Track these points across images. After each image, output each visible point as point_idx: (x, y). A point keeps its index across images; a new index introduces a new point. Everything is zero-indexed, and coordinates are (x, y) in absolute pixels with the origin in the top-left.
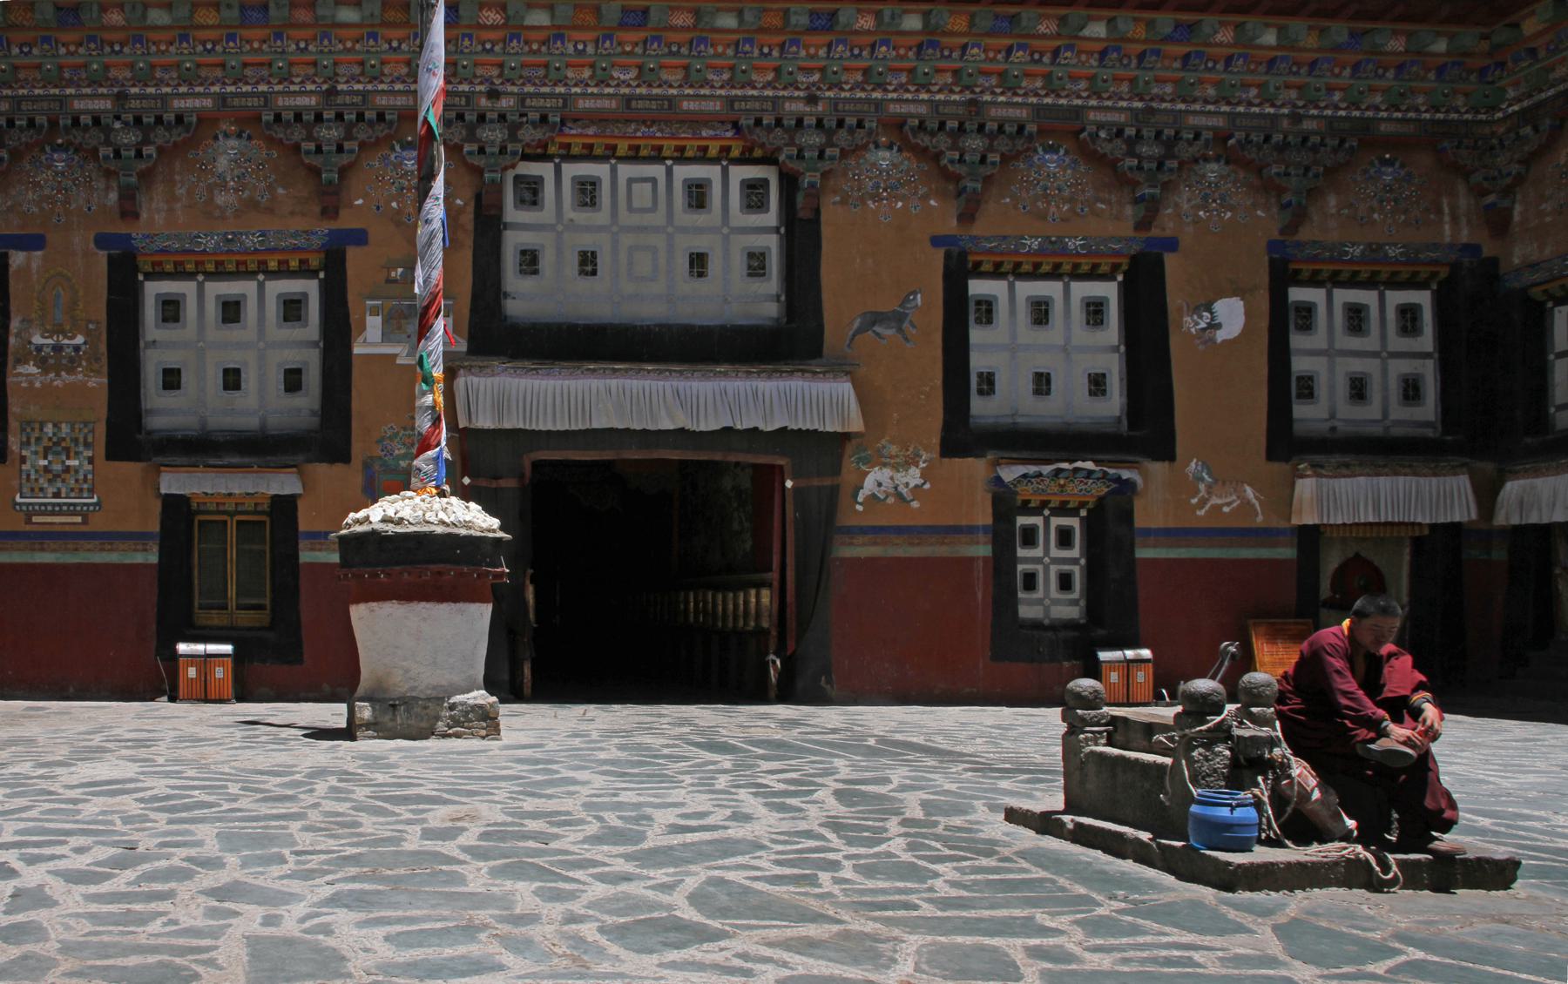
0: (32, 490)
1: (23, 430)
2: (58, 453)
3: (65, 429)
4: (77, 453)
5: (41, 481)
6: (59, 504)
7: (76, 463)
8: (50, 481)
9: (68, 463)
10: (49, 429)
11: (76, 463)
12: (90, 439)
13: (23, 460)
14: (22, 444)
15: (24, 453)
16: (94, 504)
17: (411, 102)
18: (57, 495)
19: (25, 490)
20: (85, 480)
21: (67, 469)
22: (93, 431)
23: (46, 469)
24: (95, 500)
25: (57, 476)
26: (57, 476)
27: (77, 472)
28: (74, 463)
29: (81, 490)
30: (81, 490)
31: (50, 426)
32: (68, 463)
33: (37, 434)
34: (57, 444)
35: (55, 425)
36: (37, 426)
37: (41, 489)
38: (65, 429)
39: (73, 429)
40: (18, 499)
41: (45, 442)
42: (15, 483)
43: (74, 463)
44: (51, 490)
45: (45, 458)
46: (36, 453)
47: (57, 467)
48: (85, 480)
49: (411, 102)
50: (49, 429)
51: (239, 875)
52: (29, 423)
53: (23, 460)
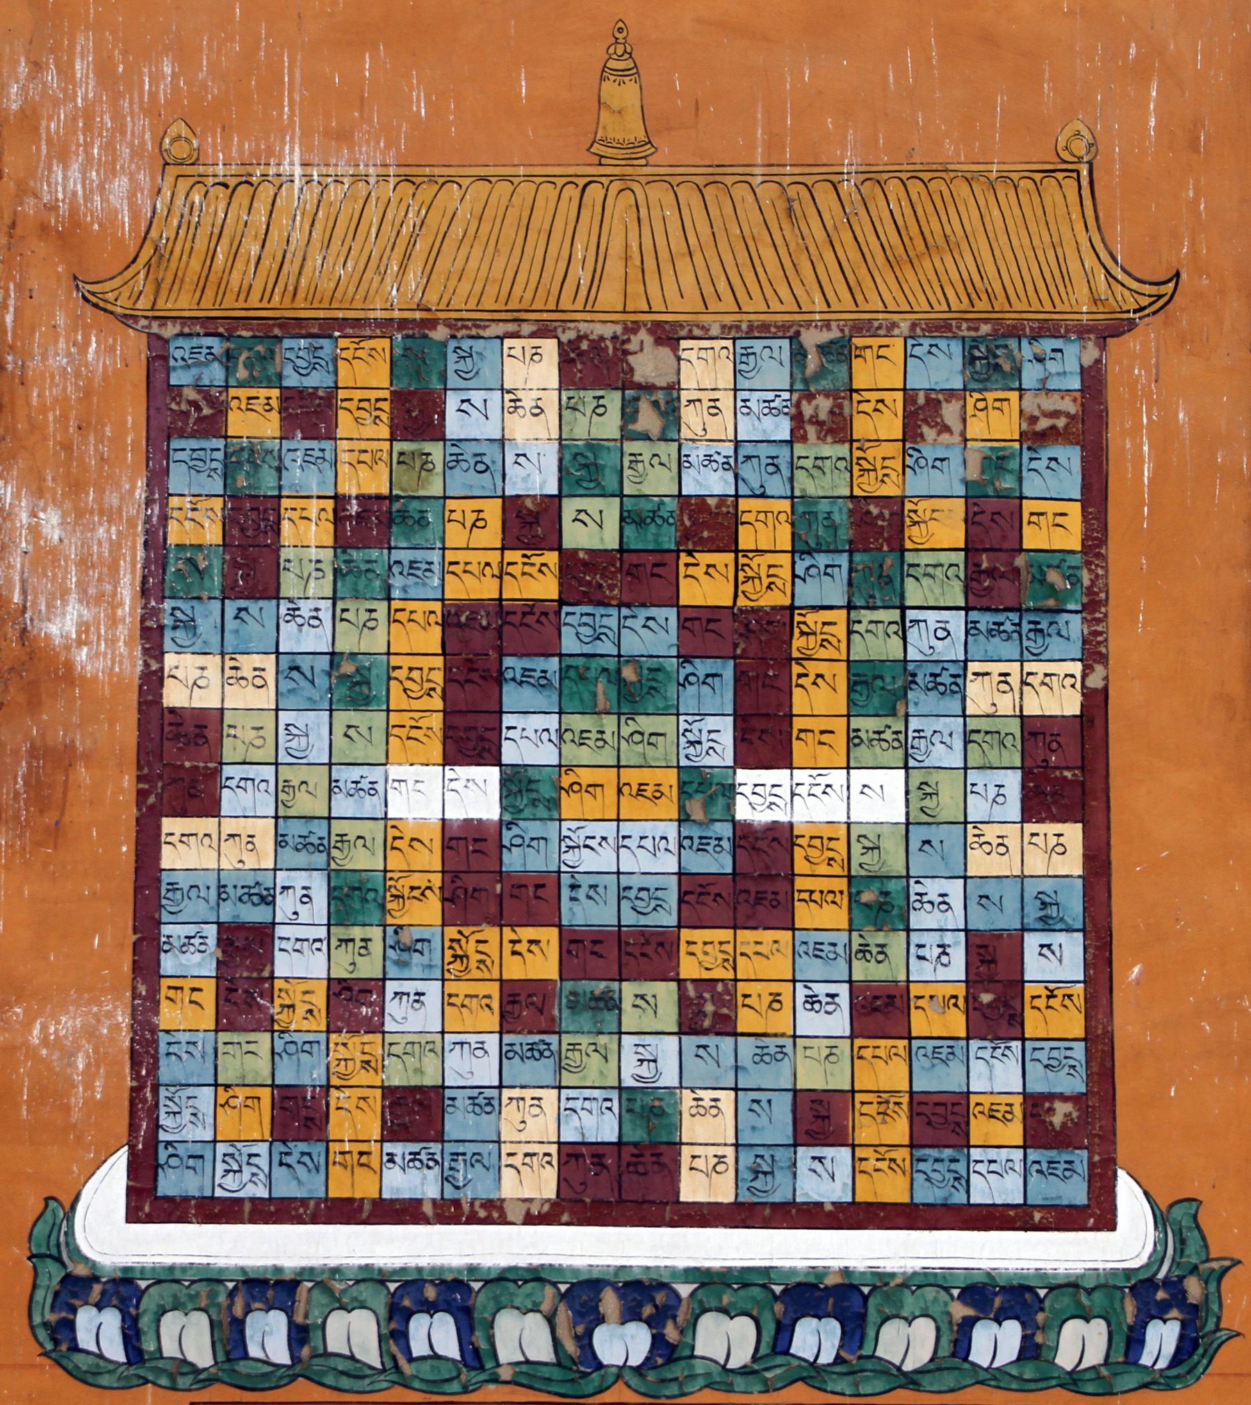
0: (298, 1116)
1: (179, 419)
2: (634, 691)
3: (724, 406)
4: (880, 689)
5: (412, 1012)
6: (644, 1295)
7: (879, 798)
8: (522, 1008)
9: (761, 797)
10: (518, 412)
11: (879, 798)
12: (1053, 528)
13: (180, 763)
14: (163, 570)
15: (191, 681)
16: (1145, 1293)
17: (692, 1189)
18: (622, 1177)
19: (186, 1122)
20: (994, 992)
21: (757, 879)
22: (1088, 426)
23: (477, 875)
24: (1130, 1241)
25: (618, 955)
26: (618, 955)
27: (881, 905)
28: (831, 797)
29: (942, 1122)
30: (942, 1122)
31: (534, 370)
32: (761, 797)
33: (363, 461)
34: (627, 575)
35: (591, 365)
36: (367, 371)
37: (415, 1113)
38: (724, 406)
39: (823, 409)
40: (104, 1229)
41: (472, 563)
42: (79, 1034)
43: (831, 797)
44: (537, 1125)
45: (471, 739)
46: (352, 683)
47: (624, 853)
48: (994, 992)
49: (692, 1189)
50: (518, 412)
51: (949, 479)
52: (253, 337)
53: (180, 763)
